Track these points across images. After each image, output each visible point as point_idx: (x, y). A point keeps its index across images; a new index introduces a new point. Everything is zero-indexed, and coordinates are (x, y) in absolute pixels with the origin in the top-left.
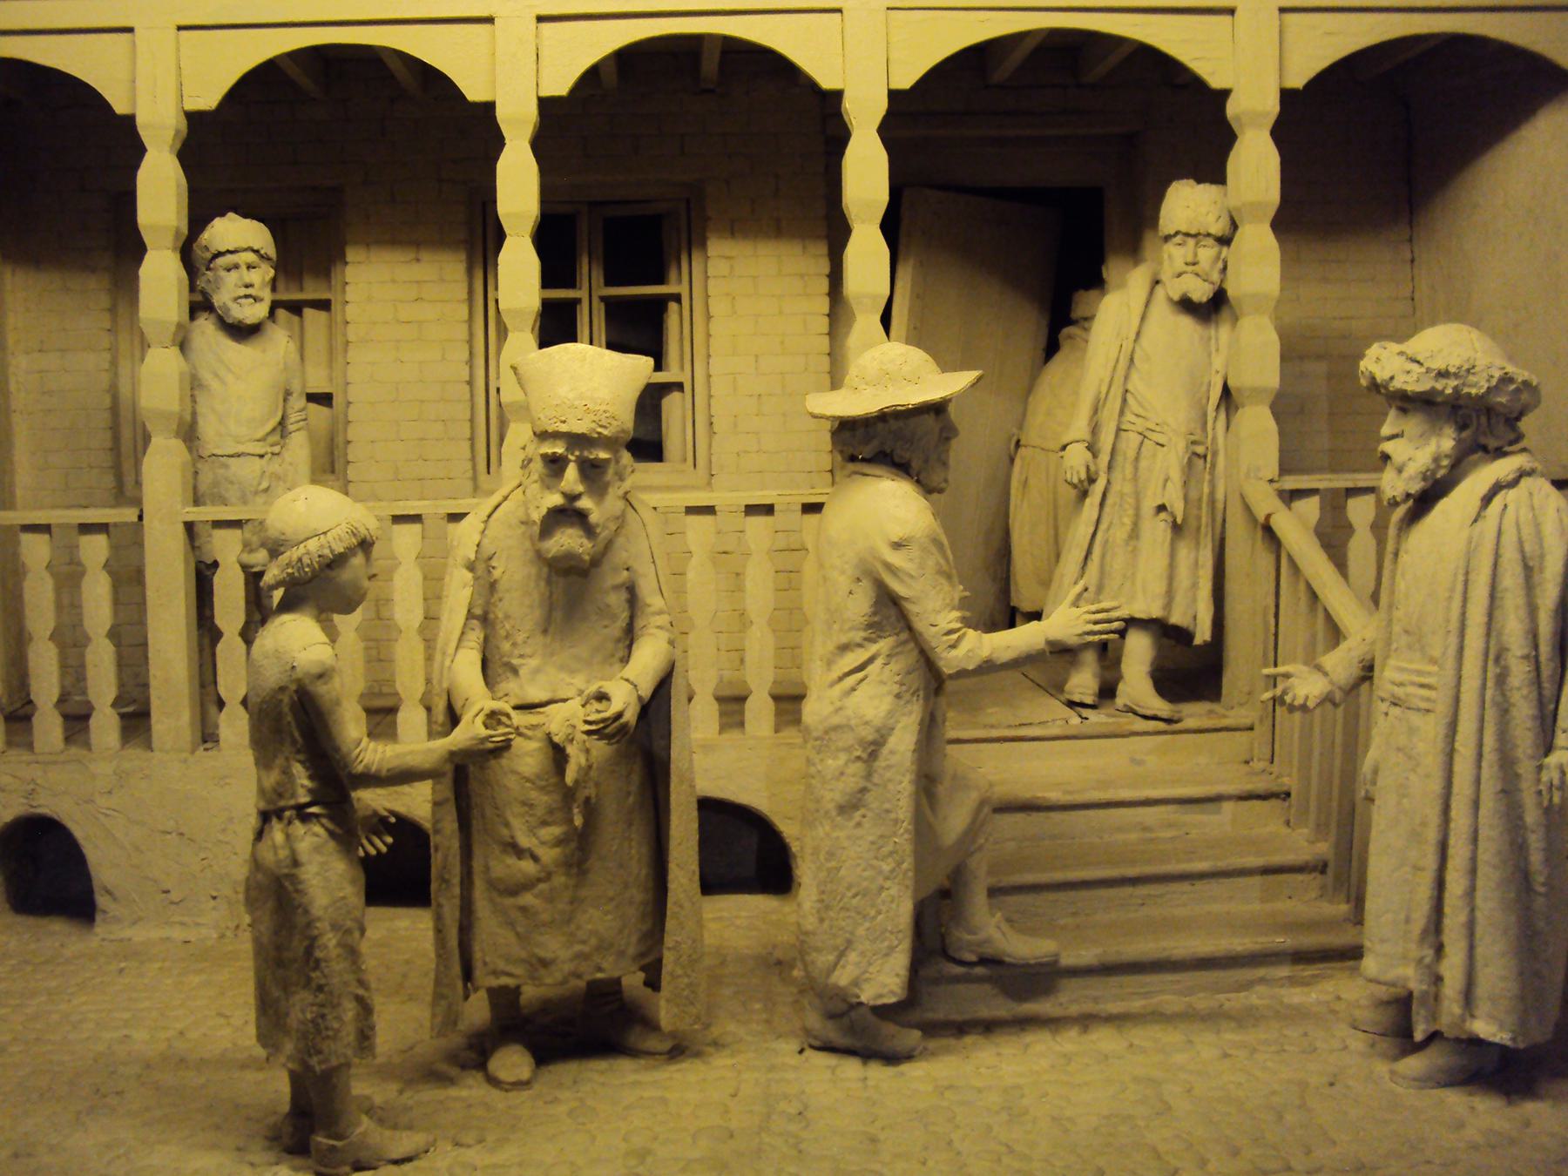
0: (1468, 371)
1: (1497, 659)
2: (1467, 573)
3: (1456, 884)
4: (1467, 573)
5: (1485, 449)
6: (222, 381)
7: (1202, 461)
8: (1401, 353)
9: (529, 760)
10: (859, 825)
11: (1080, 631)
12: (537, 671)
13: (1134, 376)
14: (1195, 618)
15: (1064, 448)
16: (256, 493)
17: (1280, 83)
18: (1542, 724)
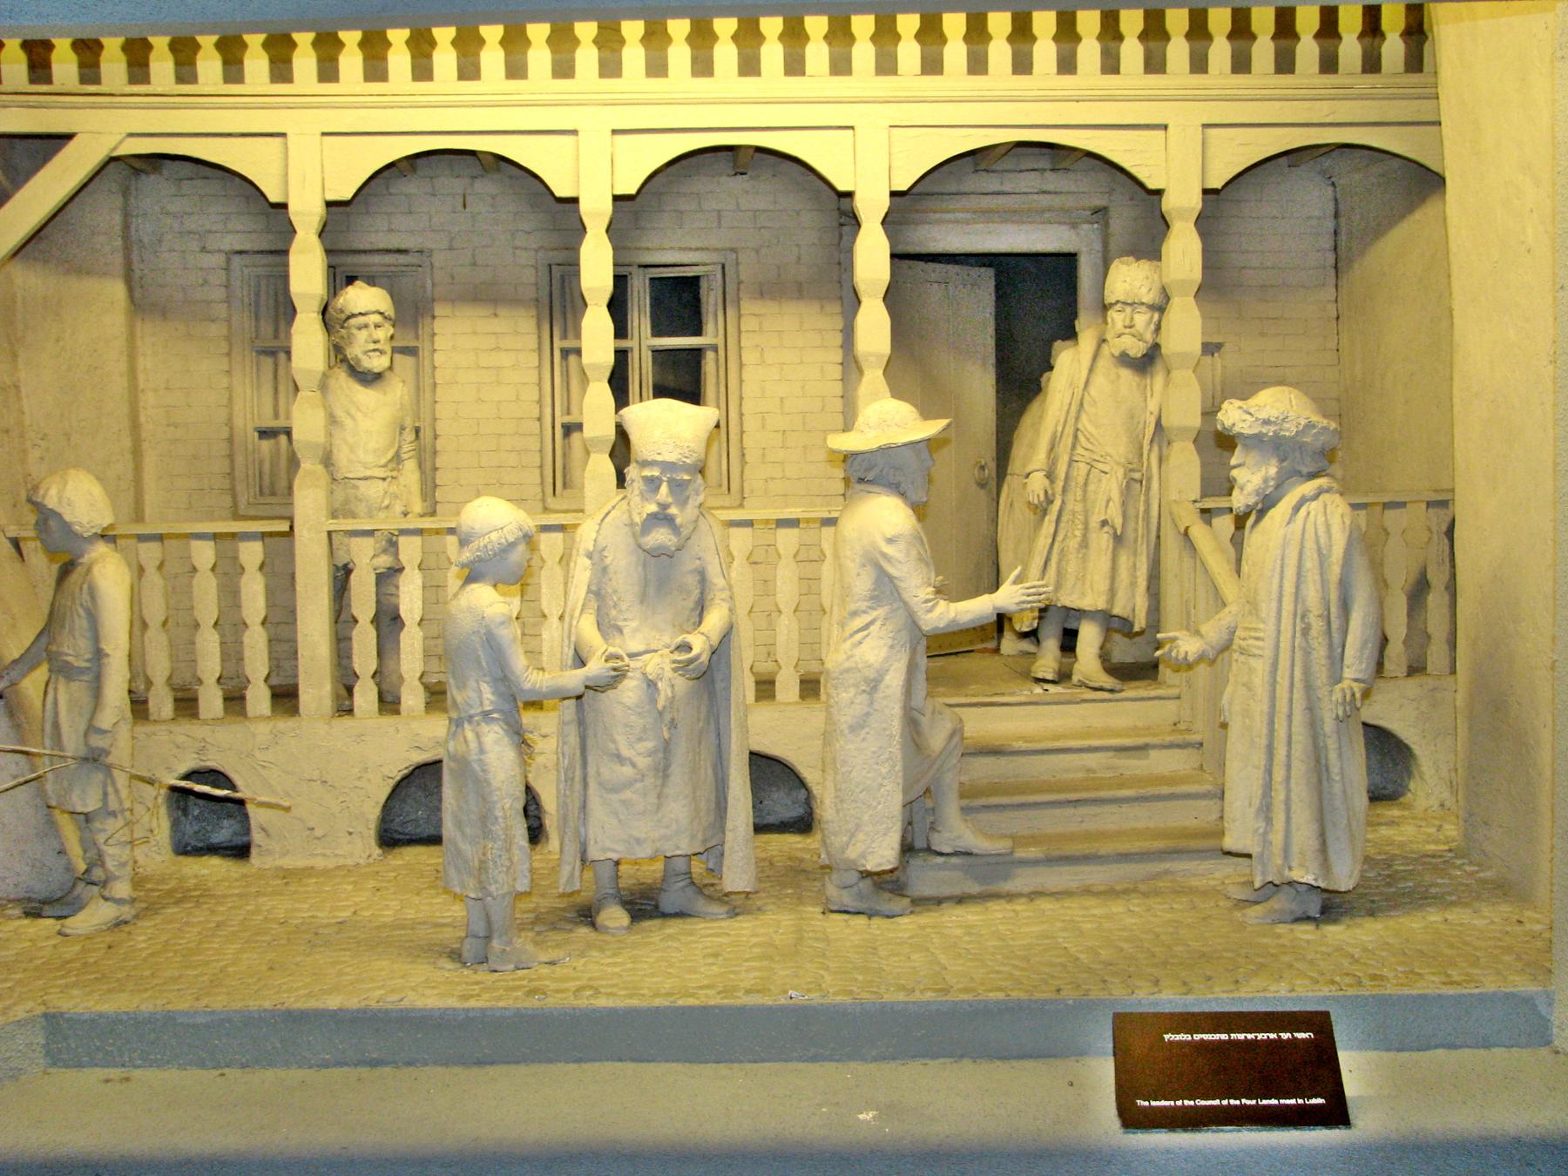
0: (1283, 420)
1: (1303, 617)
2: (1283, 560)
3: (1279, 775)
4: (1283, 560)
5: (1299, 474)
6: (353, 418)
7: (1138, 485)
8: (1240, 408)
9: (630, 694)
10: (864, 739)
11: (1017, 600)
12: (636, 630)
13: (1084, 418)
14: (1134, 610)
15: (1027, 476)
16: (380, 509)
17: (1203, 181)
18: (1332, 664)
